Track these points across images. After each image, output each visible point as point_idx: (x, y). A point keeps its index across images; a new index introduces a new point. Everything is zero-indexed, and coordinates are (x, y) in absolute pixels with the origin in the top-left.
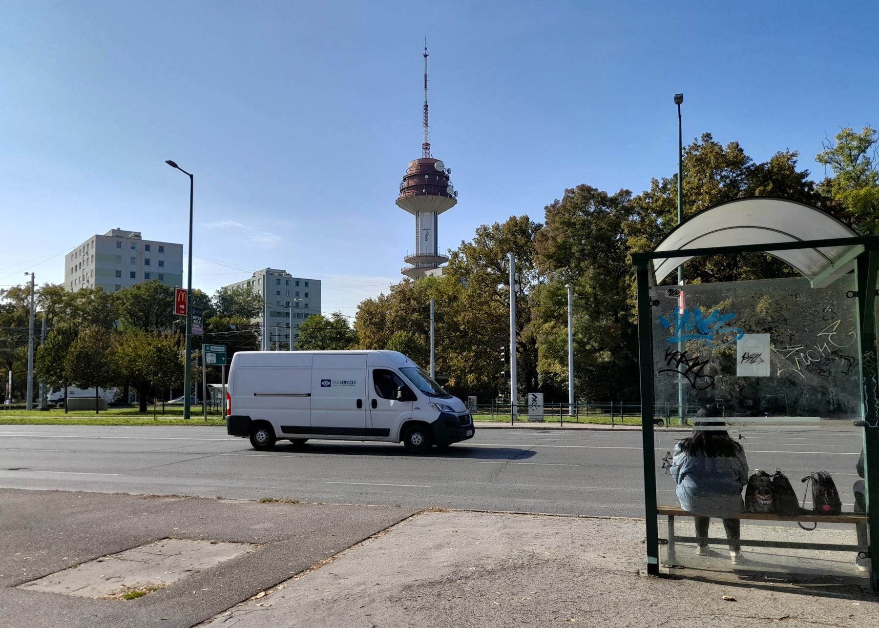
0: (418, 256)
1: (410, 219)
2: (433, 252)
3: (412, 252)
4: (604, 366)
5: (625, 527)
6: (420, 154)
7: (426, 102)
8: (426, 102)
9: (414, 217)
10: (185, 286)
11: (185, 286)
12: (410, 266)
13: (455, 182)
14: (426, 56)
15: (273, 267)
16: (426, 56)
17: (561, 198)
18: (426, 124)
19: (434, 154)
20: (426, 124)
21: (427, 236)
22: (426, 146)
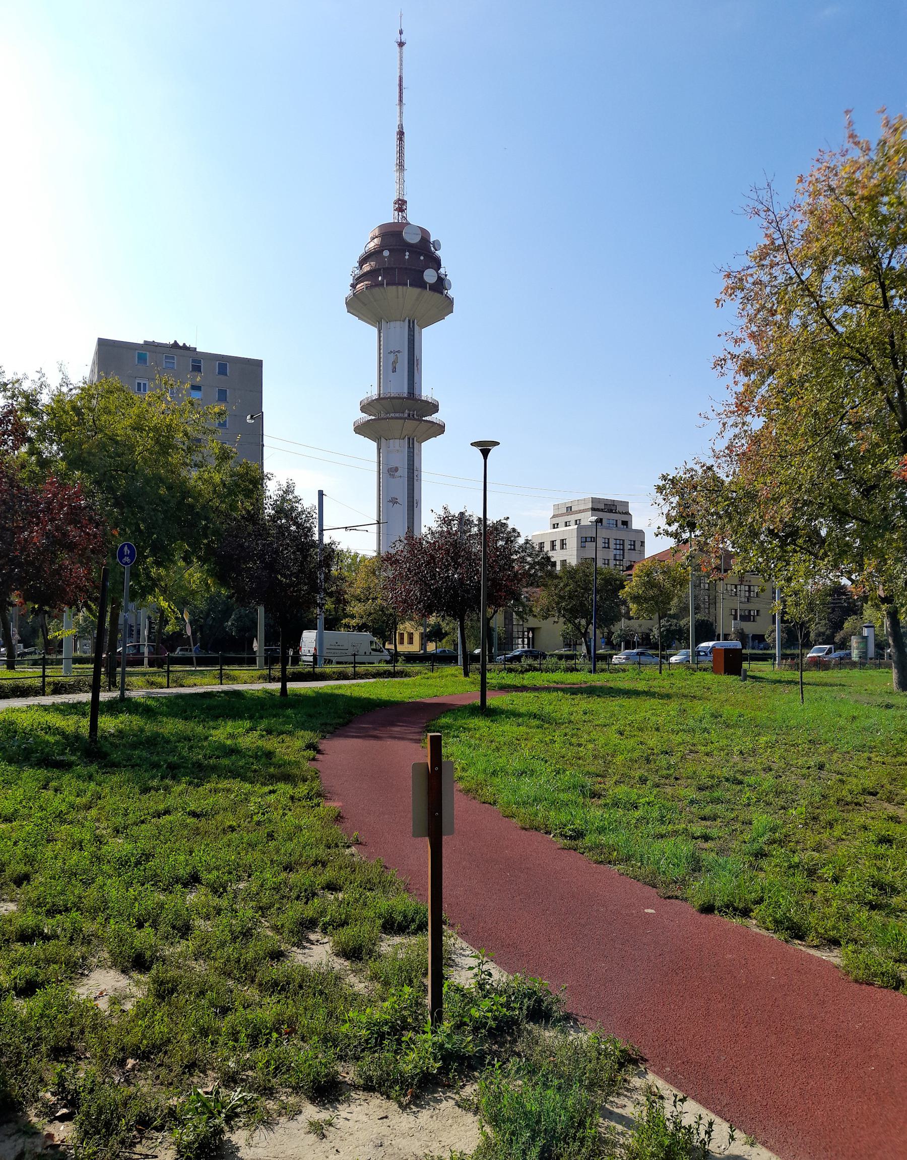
0: (379, 399)
1: (366, 336)
2: (406, 391)
3: (373, 392)
4: (78, 470)
5: (507, 728)
6: (390, 216)
7: (401, 126)
8: (401, 126)
9: (375, 330)
10: (316, 537)
11: (316, 537)
12: (366, 417)
13: (452, 263)
14: (401, 44)
15: (133, 332)
16: (401, 44)
17: (339, 547)
18: (401, 166)
19: (415, 217)
20: (401, 166)
21: (395, 362)
22: (401, 205)
